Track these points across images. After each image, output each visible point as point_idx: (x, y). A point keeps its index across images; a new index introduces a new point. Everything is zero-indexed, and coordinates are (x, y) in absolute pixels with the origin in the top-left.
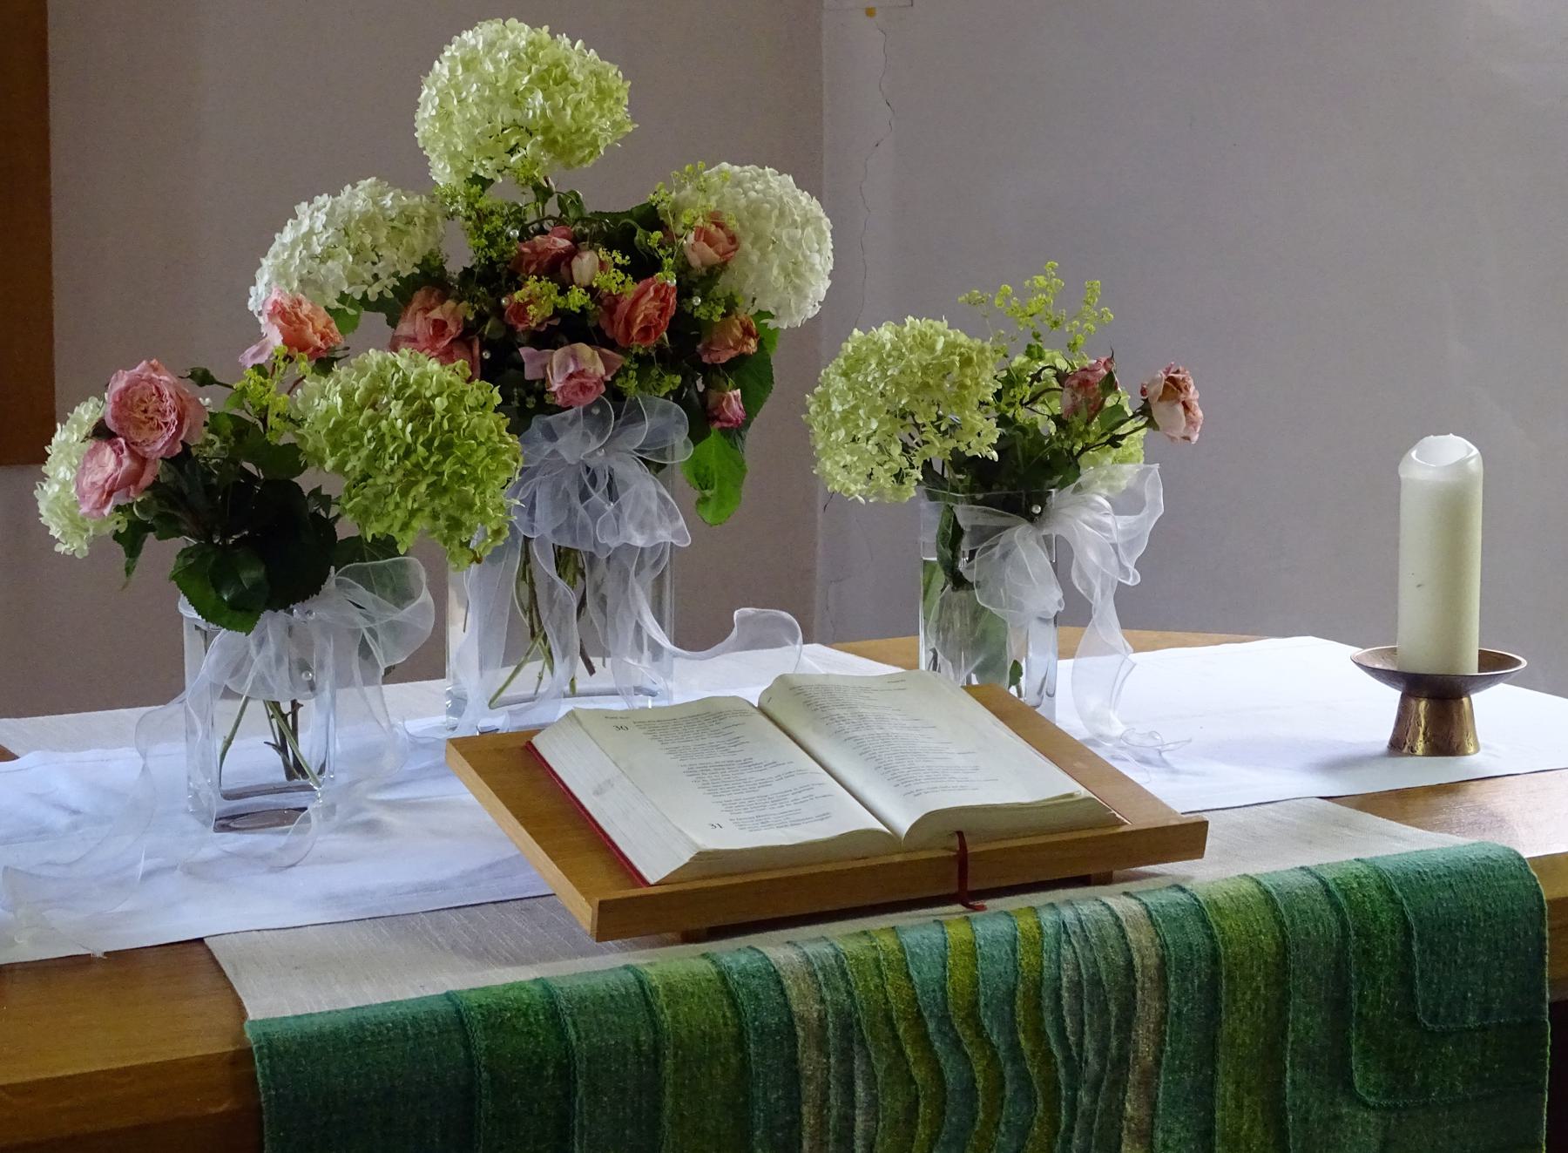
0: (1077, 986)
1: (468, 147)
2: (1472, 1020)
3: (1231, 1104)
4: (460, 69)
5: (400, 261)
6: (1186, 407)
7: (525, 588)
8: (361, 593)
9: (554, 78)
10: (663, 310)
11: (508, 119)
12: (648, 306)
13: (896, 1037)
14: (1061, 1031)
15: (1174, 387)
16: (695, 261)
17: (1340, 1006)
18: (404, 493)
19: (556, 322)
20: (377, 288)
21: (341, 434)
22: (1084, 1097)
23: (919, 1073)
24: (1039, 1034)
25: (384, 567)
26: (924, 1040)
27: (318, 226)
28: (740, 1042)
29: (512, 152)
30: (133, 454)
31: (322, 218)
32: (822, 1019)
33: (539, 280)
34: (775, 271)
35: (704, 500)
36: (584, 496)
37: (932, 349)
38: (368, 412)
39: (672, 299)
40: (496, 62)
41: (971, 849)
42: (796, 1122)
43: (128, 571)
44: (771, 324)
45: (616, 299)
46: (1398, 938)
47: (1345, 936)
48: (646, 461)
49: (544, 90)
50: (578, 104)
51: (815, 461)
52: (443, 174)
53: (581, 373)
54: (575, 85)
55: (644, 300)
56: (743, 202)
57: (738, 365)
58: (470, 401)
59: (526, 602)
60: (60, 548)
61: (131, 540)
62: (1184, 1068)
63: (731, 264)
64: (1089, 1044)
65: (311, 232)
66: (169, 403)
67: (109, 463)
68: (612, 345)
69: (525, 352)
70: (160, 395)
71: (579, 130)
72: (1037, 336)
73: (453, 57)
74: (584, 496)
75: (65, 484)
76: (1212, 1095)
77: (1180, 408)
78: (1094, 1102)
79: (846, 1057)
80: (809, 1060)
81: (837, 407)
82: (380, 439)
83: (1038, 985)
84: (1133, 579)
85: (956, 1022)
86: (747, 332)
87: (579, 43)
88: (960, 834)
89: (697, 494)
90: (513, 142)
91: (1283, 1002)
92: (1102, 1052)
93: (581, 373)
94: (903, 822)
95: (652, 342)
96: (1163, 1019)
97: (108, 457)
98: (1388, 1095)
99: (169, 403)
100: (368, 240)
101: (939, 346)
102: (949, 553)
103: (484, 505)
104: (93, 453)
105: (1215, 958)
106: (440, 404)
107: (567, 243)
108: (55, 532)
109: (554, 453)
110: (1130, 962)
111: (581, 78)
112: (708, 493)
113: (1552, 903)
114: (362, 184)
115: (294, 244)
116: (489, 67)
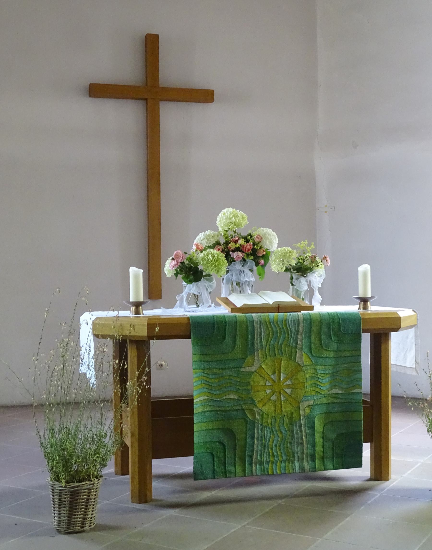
0: (291, 321)
1: (224, 225)
2: (350, 333)
3: (314, 339)
4: (223, 215)
5: (213, 241)
6: (327, 260)
7: (232, 288)
8: (206, 281)
9: (235, 216)
10: (251, 247)
11: (229, 221)
12: (248, 247)
13: (267, 324)
14: (289, 327)
15: (325, 258)
16: (256, 241)
17: (329, 328)
18: (211, 266)
19: (235, 249)
20: (210, 244)
21: (203, 259)
22: (293, 335)
23: (270, 329)
24: (286, 326)
25: (208, 278)
26: (270, 325)
27: (202, 236)
28: (247, 322)
29: (230, 226)
30: (177, 261)
31: (202, 235)
32: (257, 321)
33: (233, 243)
34: (268, 242)
35: (260, 278)
36: (240, 274)
37: (286, 250)
38: (207, 256)
39: (252, 246)
40: (228, 214)
41: (280, 306)
42: (254, 333)
43: (176, 279)
44: (268, 250)
45: (244, 246)
46: (338, 320)
47: (330, 319)
48: (249, 269)
49: (234, 217)
50: (239, 219)
51: (271, 267)
52: (220, 229)
53: (238, 255)
54: (239, 217)
55: (248, 246)
56: (263, 233)
57: (263, 256)
58: (220, 255)
59: (232, 290)
60: (167, 276)
61: (176, 275)
62: (306, 333)
63: (261, 242)
64: (293, 329)
65: (201, 237)
66: (181, 255)
67: (174, 263)
68: (243, 252)
69: (231, 253)
70: (180, 254)
71: (239, 223)
72: (304, 250)
73: (222, 213)
74: (240, 274)
75: (168, 267)
76: (311, 337)
77: (326, 261)
78: (294, 336)
79: (260, 326)
80: (256, 325)
81: (273, 259)
82: (208, 260)
83: (286, 320)
84: (320, 286)
85: (275, 323)
86: (264, 251)
87: (241, 211)
88: (279, 305)
89: (259, 277)
90: (230, 225)
91: (321, 327)
92: (295, 329)
93: (238, 255)
94: (271, 303)
95: (249, 252)
96: (303, 326)
97: (174, 262)
98: (338, 341)
99: (181, 255)
100: (209, 238)
101: (287, 250)
102: (291, 281)
103: (222, 269)
104: (172, 262)
105: (311, 319)
106: (216, 255)
107: (238, 239)
108: (166, 274)
109: (235, 268)
110: (299, 319)
111: (239, 216)
112: (261, 277)
113: (362, 318)
114: (208, 231)
115: (199, 239)
116: (227, 214)
